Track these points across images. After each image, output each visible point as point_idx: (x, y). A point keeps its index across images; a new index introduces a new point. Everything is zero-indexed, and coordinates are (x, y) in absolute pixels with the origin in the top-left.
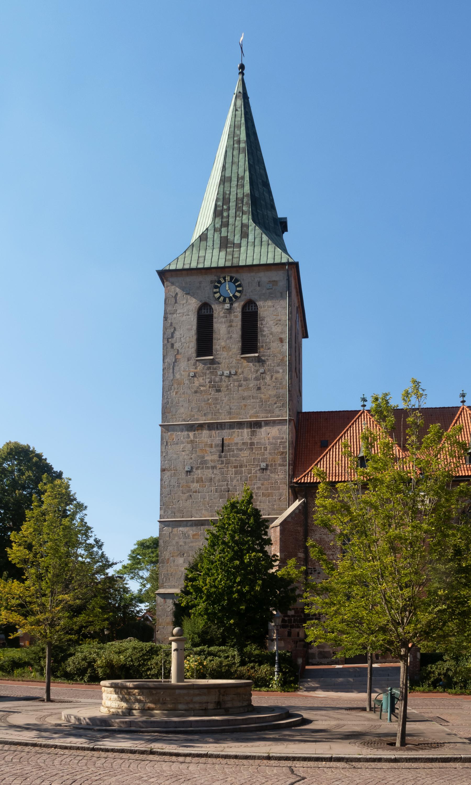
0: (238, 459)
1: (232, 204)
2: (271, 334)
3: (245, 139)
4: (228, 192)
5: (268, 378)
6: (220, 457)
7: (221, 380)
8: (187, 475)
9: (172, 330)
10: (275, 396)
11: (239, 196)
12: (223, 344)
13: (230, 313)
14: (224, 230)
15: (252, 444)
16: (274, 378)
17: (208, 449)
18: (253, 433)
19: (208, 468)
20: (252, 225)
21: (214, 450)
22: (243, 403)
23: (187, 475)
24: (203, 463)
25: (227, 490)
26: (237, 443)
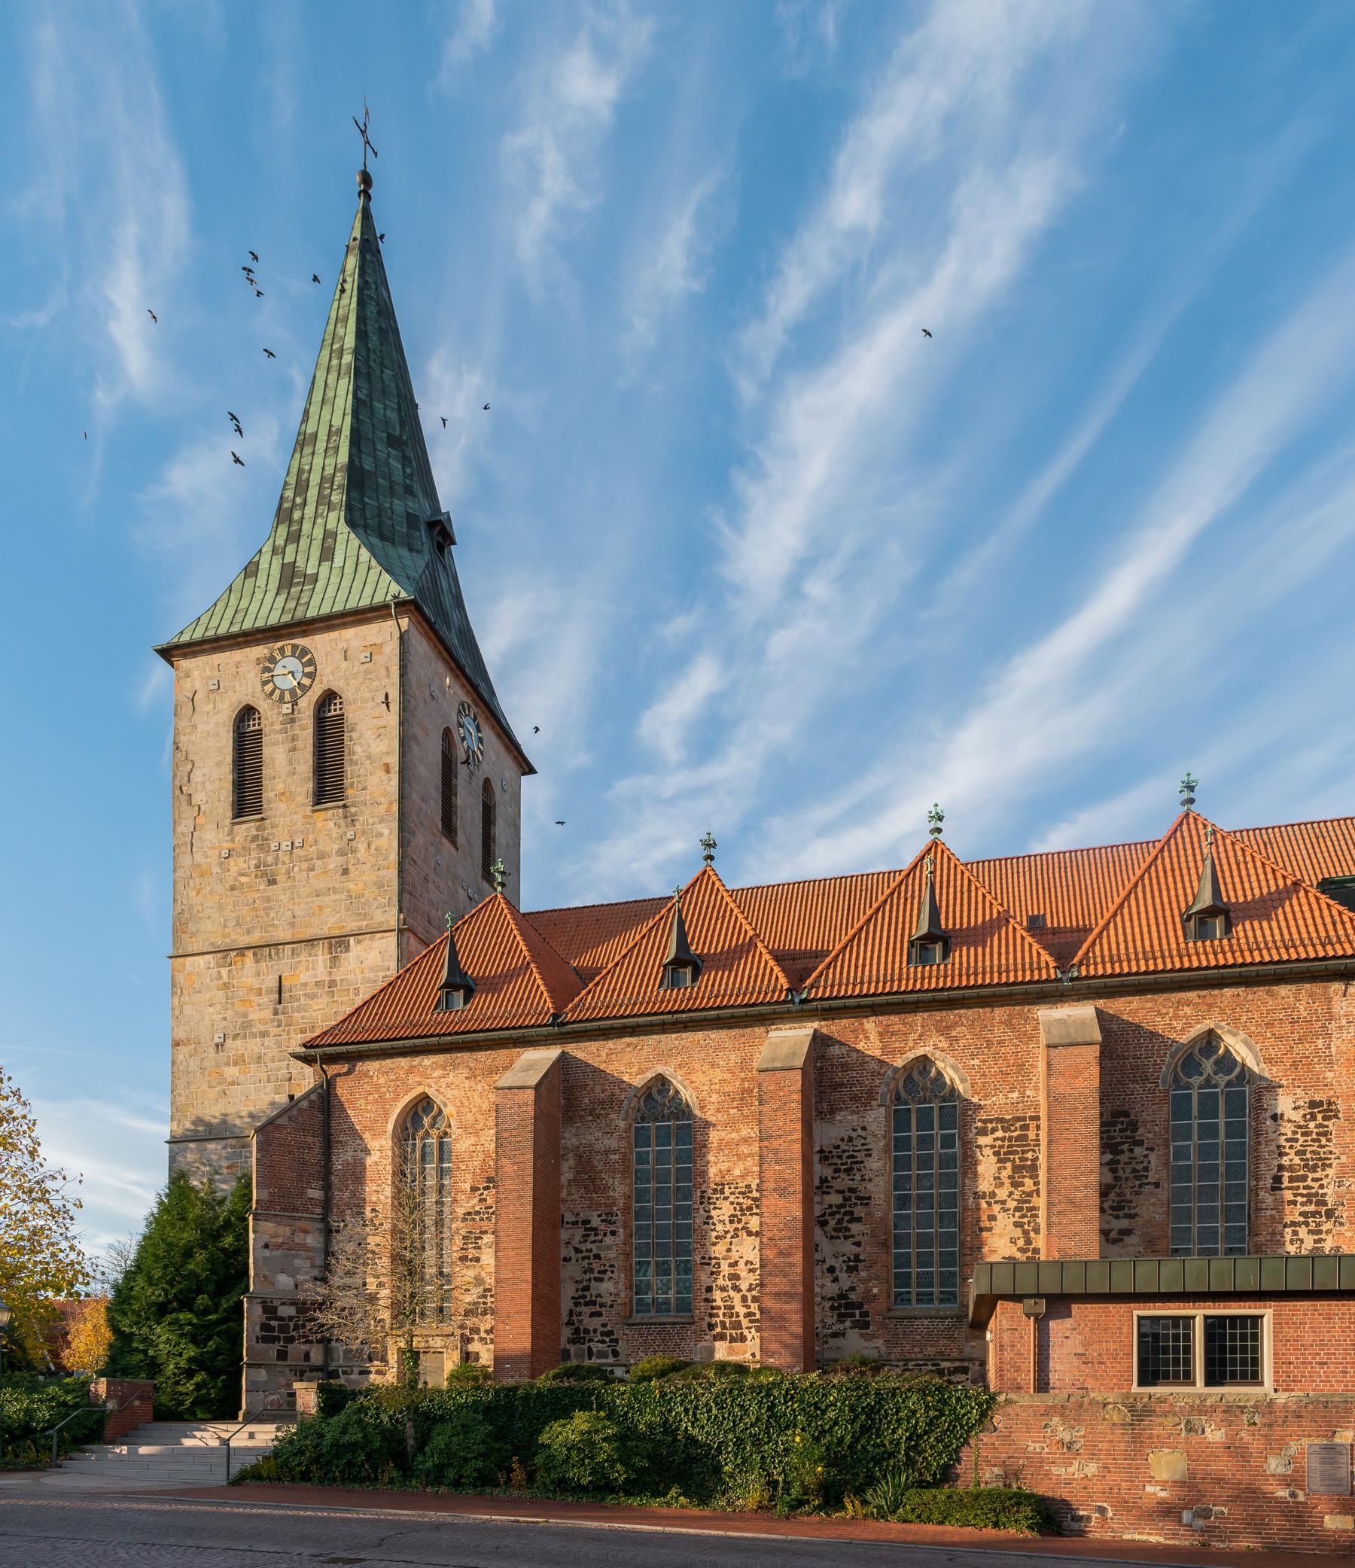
0: (307, 1014)
1: (312, 494)
2: (369, 757)
3: (353, 344)
4: (307, 468)
5: (362, 848)
6: (276, 1013)
7: (277, 859)
8: (217, 1052)
9: (190, 766)
10: (375, 884)
11: (326, 473)
12: (280, 787)
13: (293, 721)
14: (291, 549)
15: (332, 984)
16: (373, 847)
17: (253, 998)
18: (334, 961)
19: (254, 1035)
20: (344, 529)
21: (264, 1000)
22: (318, 901)
23: (217, 1052)
24: (244, 1030)
25: (288, 1076)
26: (306, 984)
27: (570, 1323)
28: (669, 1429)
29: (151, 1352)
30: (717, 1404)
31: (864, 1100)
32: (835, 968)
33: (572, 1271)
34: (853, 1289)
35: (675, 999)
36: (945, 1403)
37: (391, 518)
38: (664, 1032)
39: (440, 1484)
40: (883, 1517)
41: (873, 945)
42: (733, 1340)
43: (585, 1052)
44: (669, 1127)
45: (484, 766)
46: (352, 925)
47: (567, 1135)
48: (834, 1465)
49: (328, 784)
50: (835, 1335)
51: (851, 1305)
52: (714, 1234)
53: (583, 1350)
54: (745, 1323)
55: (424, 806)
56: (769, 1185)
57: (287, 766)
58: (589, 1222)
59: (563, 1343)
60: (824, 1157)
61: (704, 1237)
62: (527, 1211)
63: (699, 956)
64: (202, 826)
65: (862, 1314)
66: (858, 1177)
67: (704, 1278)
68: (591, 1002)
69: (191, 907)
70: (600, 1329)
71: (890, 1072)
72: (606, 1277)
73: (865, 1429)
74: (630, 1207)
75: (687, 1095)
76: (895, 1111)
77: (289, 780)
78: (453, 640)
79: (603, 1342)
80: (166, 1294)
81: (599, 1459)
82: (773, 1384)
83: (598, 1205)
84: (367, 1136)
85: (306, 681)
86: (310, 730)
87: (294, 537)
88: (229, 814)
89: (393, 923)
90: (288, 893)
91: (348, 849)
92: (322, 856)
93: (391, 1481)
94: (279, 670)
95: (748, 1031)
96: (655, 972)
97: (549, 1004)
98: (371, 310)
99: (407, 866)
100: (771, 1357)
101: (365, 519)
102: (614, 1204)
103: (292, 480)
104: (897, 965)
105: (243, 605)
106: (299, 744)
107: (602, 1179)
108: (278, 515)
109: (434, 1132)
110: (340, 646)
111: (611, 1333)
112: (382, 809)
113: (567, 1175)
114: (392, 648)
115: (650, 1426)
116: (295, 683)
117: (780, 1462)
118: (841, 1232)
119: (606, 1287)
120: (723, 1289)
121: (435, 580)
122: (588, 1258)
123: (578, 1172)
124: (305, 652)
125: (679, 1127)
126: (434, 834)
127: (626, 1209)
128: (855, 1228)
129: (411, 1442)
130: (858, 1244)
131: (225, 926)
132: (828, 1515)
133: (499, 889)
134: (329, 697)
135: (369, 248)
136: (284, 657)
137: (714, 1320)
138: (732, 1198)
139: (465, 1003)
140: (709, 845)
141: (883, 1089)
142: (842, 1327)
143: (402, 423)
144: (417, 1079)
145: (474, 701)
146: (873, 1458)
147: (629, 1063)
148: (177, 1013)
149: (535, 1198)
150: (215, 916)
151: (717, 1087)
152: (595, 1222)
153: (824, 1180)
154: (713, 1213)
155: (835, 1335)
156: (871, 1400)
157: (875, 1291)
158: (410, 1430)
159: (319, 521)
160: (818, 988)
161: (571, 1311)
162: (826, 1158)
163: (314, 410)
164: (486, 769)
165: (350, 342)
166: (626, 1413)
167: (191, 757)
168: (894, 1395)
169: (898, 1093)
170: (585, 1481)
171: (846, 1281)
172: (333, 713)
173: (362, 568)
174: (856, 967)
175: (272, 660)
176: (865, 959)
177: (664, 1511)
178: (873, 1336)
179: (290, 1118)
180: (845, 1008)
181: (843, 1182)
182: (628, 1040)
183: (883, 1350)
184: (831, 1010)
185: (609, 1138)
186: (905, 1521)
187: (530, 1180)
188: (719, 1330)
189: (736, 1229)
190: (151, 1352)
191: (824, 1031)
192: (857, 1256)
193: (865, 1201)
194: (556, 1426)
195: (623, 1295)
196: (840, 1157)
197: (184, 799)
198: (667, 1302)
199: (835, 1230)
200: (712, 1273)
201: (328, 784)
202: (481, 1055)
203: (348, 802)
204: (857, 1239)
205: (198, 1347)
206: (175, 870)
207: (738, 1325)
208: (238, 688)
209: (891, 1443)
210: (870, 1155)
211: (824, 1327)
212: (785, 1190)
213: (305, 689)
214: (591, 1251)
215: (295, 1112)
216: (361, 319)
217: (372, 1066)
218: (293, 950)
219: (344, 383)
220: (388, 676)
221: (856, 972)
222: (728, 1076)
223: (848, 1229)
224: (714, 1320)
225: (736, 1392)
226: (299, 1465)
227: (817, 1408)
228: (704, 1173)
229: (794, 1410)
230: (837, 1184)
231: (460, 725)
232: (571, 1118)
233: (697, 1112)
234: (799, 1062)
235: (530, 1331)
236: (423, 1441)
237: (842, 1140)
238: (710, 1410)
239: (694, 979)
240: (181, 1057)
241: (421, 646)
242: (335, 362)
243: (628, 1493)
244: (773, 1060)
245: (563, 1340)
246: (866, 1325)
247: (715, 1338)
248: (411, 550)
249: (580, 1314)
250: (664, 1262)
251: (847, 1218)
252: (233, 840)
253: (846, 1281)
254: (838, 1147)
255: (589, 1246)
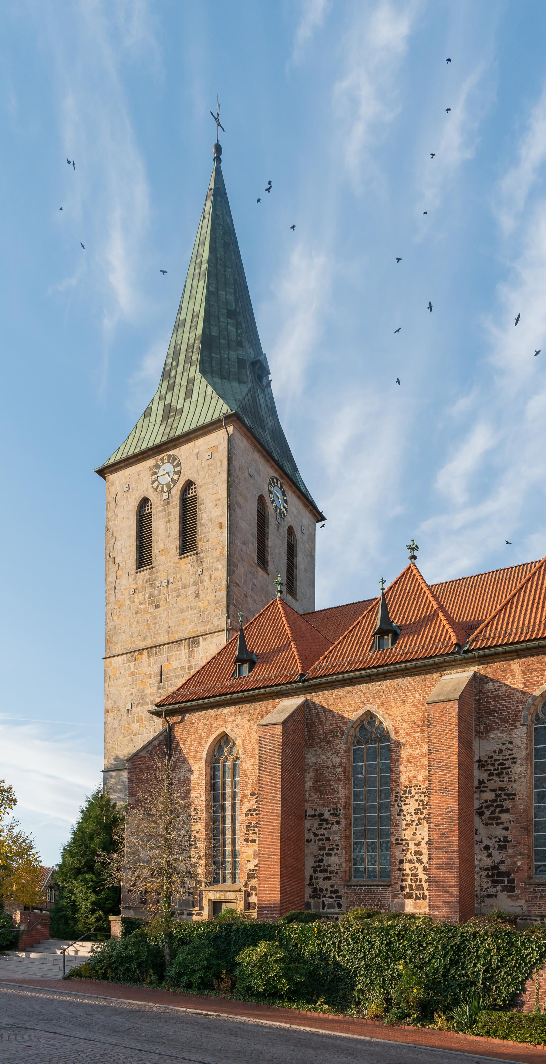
3: (207, 257)
4: (180, 342)
5: (206, 578)
6: (159, 689)
7: (160, 592)
8: (128, 715)
9: (114, 540)
12: (161, 546)
16: (213, 578)
20: (199, 375)
26: (175, 669)
27: (311, 884)
28: (324, 957)
29: (73, 898)
30: (353, 939)
31: (511, 721)
32: (492, 626)
33: (312, 849)
34: (502, 862)
35: (378, 657)
36: (512, 944)
37: (228, 364)
38: (371, 681)
39: (178, 986)
40: (462, 1030)
41: (522, 606)
42: (417, 898)
43: (322, 699)
44: (375, 747)
45: (289, 518)
46: (201, 629)
47: (309, 756)
48: (431, 989)
49: (188, 542)
50: (489, 896)
51: (501, 874)
52: (404, 822)
53: (319, 903)
54: (426, 886)
55: (244, 548)
56: (435, 786)
57: (165, 531)
58: (322, 815)
59: (307, 898)
60: (482, 765)
61: (397, 825)
62: (277, 807)
63: (399, 626)
64: (120, 576)
65: (509, 881)
66: (506, 779)
67: (398, 854)
68: (326, 664)
69: (115, 627)
70: (330, 889)
71: (530, 700)
72: (333, 853)
73: (453, 962)
74: (349, 804)
75: (387, 724)
76: (536, 729)
77: (166, 541)
78: (267, 437)
79: (332, 898)
80: (80, 863)
81: (272, 974)
82: (391, 926)
83: (329, 803)
84: (191, 761)
85: (176, 477)
86: (178, 508)
87: (171, 388)
88: (135, 567)
89: (224, 626)
90: (166, 612)
91: (199, 581)
92: (184, 587)
93: (151, 983)
94: (161, 472)
95: (428, 676)
96: (368, 638)
97: (299, 668)
98: (220, 232)
99: (232, 588)
100: (437, 910)
101: (212, 367)
102: (338, 802)
103: (171, 352)
104: (538, 619)
105: (142, 435)
106: (172, 517)
107: (331, 785)
108: (163, 375)
109: (231, 758)
110: (194, 451)
111: (336, 891)
112: (218, 552)
113: (309, 783)
114: (224, 447)
115: (312, 954)
116: (170, 479)
117: (396, 984)
118: (494, 820)
119: (334, 860)
120: (411, 862)
121: (255, 399)
122: (322, 840)
123: (316, 781)
124: (175, 458)
125: (383, 748)
126: (251, 566)
127: (347, 806)
128: (504, 817)
129: (167, 957)
130: (506, 829)
131: (132, 637)
132: (423, 1025)
133: (279, 595)
134: (189, 484)
135: (219, 195)
136: (163, 464)
137: (404, 884)
138: (416, 797)
139: (249, 672)
140: (413, 549)
141: (525, 713)
142: (494, 890)
143: (236, 301)
144: (220, 723)
145: (281, 476)
146: (459, 985)
147: (347, 704)
148: (107, 692)
149: (283, 799)
150: (127, 631)
151: (406, 717)
152: (327, 815)
153: (481, 782)
154: (404, 808)
155: (489, 896)
156: (458, 941)
157: (519, 864)
158: (167, 951)
159: (185, 374)
160: (478, 641)
161: (311, 876)
162: (483, 766)
163: (185, 305)
164: (290, 520)
165: (206, 256)
166: (297, 944)
167: (115, 534)
168: (475, 938)
169: (537, 715)
170: (261, 989)
171: (497, 856)
172: (191, 495)
173: (208, 399)
174: (508, 623)
175: (157, 467)
176: (514, 617)
177: (311, 1014)
178: (518, 898)
179: (147, 752)
180: (496, 654)
181: (496, 783)
182: (347, 688)
183: (525, 908)
184: (486, 657)
185: (334, 757)
186: (477, 1035)
187: (280, 787)
188: (407, 890)
189: (420, 819)
190: (73, 898)
191: (482, 672)
192: (506, 838)
193: (512, 796)
194: (247, 950)
195: (344, 865)
196: (493, 765)
197: (111, 560)
198: (374, 871)
199: (489, 818)
200: (403, 850)
201: (188, 542)
202: (257, 705)
203: (199, 551)
204: (505, 825)
205: (97, 895)
206: (106, 605)
207: (420, 888)
208: (139, 487)
209: (472, 974)
210: (515, 763)
211: (481, 890)
212: (446, 788)
213: (174, 481)
214: (324, 835)
215: (150, 748)
216: (213, 240)
217: (193, 717)
218: (168, 648)
219: (201, 283)
220: (221, 466)
221: (507, 627)
222: (414, 710)
223: (499, 818)
224: (404, 884)
225: (366, 931)
226: (101, 969)
227: (420, 945)
228: (398, 779)
229: (404, 946)
230: (491, 785)
231: (271, 492)
232: (311, 744)
233: (393, 736)
234: (457, 695)
235: (279, 889)
236: (173, 956)
237: (495, 752)
238: (349, 944)
239: (393, 643)
240: (109, 719)
241: (243, 443)
242: (197, 271)
243: (291, 1000)
244: (439, 695)
245: (307, 895)
246: (512, 889)
247: (406, 896)
248: (240, 382)
249: (317, 878)
250: (372, 843)
251: (498, 810)
252: (136, 583)
253: (497, 856)
254: (492, 757)
255: (323, 831)
